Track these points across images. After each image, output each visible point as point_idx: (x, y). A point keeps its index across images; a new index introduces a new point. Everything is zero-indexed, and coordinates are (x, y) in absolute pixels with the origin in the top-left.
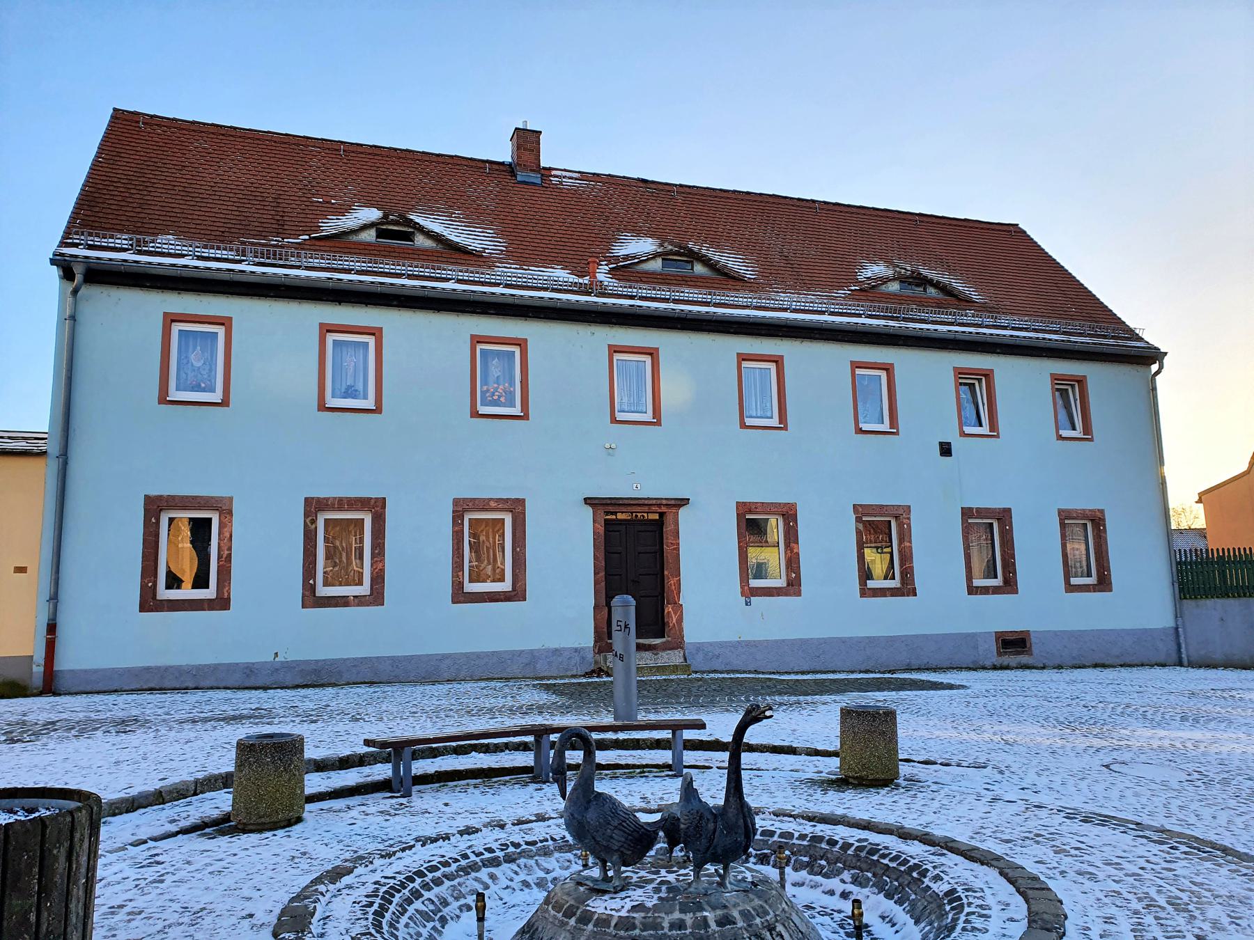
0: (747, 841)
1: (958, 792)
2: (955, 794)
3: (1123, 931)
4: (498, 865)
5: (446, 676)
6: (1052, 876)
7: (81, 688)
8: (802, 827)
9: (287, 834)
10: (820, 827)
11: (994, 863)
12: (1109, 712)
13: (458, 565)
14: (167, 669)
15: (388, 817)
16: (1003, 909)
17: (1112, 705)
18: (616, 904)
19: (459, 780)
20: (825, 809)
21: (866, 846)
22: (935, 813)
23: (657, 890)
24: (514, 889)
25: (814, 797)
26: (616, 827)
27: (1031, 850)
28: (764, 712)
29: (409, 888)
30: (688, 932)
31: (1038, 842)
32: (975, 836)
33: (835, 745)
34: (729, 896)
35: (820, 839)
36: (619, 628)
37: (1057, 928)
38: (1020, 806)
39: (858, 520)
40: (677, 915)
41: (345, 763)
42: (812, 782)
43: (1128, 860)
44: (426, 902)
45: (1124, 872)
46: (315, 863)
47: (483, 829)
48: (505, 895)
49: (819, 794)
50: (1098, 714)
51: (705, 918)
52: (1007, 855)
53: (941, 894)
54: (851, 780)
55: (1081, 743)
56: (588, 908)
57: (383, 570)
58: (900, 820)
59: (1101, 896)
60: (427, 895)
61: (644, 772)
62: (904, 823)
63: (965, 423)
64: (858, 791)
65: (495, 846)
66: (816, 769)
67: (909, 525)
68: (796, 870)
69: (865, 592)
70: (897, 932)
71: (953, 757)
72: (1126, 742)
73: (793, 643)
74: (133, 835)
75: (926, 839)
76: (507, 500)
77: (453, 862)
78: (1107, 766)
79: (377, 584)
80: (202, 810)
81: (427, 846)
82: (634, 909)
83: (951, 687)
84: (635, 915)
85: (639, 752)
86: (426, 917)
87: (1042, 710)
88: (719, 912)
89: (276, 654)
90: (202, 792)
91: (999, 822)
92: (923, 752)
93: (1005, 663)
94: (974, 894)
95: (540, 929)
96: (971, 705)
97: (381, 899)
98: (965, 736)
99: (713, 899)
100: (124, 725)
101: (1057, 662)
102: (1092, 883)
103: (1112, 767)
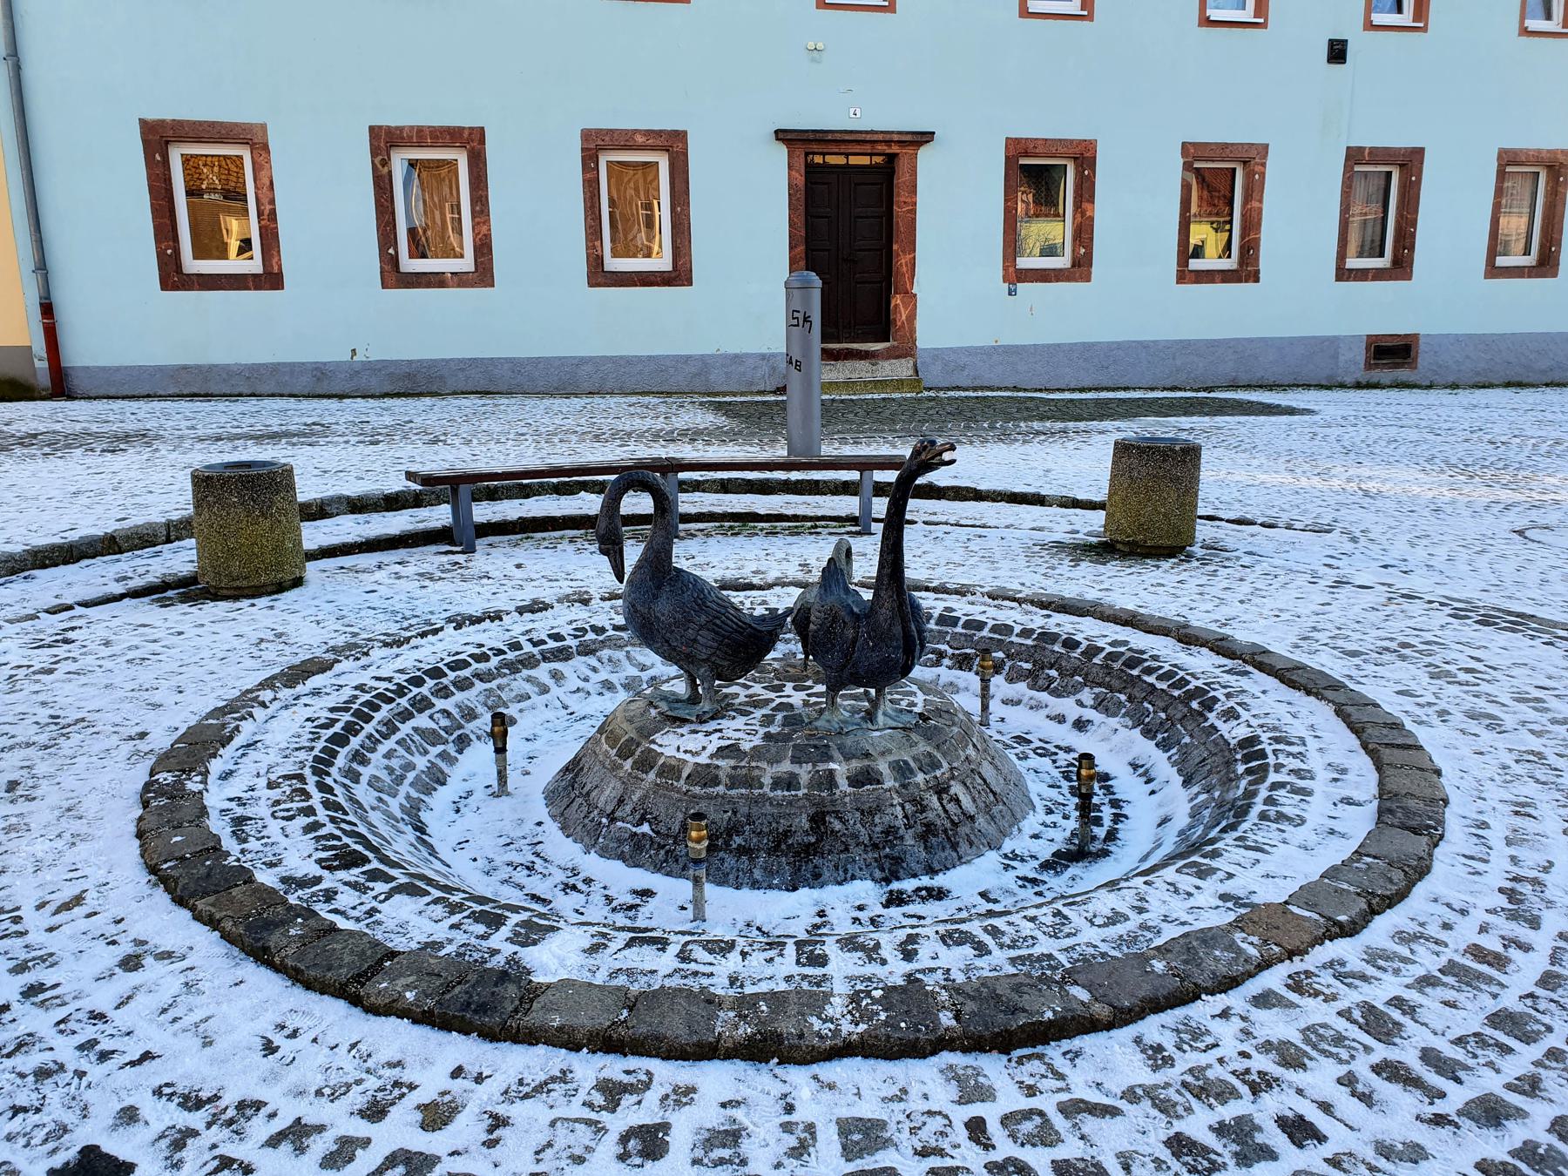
0: (908, 659)
1: (1283, 568)
2: (1279, 571)
3: (1549, 833)
4: (567, 659)
5: (586, 386)
6: (1425, 718)
7: (102, 392)
8: (1029, 617)
9: (271, 604)
10: (1058, 618)
11: (1328, 693)
12: (1527, 451)
13: (594, 232)
14: (212, 368)
15: (427, 583)
16: (1336, 780)
17: (1533, 441)
18: (693, 742)
19: (554, 530)
20: (1069, 591)
21: (1123, 654)
22: (1242, 602)
23: (768, 720)
24: (588, 693)
25: (1057, 571)
26: (701, 627)
27: (1391, 671)
28: (941, 454)
29: (410, 695)
30: (800, 793)
31: (1403, 658)
32: (1301, 643)
33: (1100, 495)
34: (877, 737)
35: (1054, 638)
36: (795, 322)
37: (1429, 827)
38: (1377, 596)
39: (1187, 167)
40: (786, 766)
41: (393, 503)
42: (1060, 546)
43: (1556, 693)
44: (436, 716)
45: (1550, 715)
46: (288, 650)
47: (555, 605)
48: (575, 703)
49: (1065, 566)
50: (1511, 454)
51: (831, 772)
52: (1350, 677)
53: (1233, 742)
54: (1119, 546)
55: (1482, 495)
56: (653, 746)
57: (488, 236)
58: (1185, 612)
59: (1509, 759)
60: (440, 704)
61: (816, 527)
62: (1190, 617)
63: (1376, 6)
64: (1127, 563)
65: (565, 631)
66: (1070, 528)
67: (1263, 175)
68: (1010, 680)
69: (1185, 276)
70: (1153, 792)
71: (1281, 514)
72: (1553, 496)
73: (1072, 347)
74: (57, 597)
75: (1221, 646)
76: (659, 133)
77: (495, 655)
78: (1521, 533)
79: (483, 255)
80: (168, 564)
81: (464, 629)
82: (721, 752)
83: (1291, 411)
84: (720, 763)
85: (818, 498)
86: (432, 737)
87: (1425, 447)
88: (856, 764)
89: (354, 350)
90: (179, 539)
91: (1343, 620)
92: (1237, 505)
93: (1375, 380)
94: (1288, 748)
95: (585, 770)
96: (1319, 438)
97: (352, 715)
98: (1304, 482)
99: (849, 741)
100: (119, 442)
101: (1451, 379)
102: (1493, 735)
103: (1528, 534)
